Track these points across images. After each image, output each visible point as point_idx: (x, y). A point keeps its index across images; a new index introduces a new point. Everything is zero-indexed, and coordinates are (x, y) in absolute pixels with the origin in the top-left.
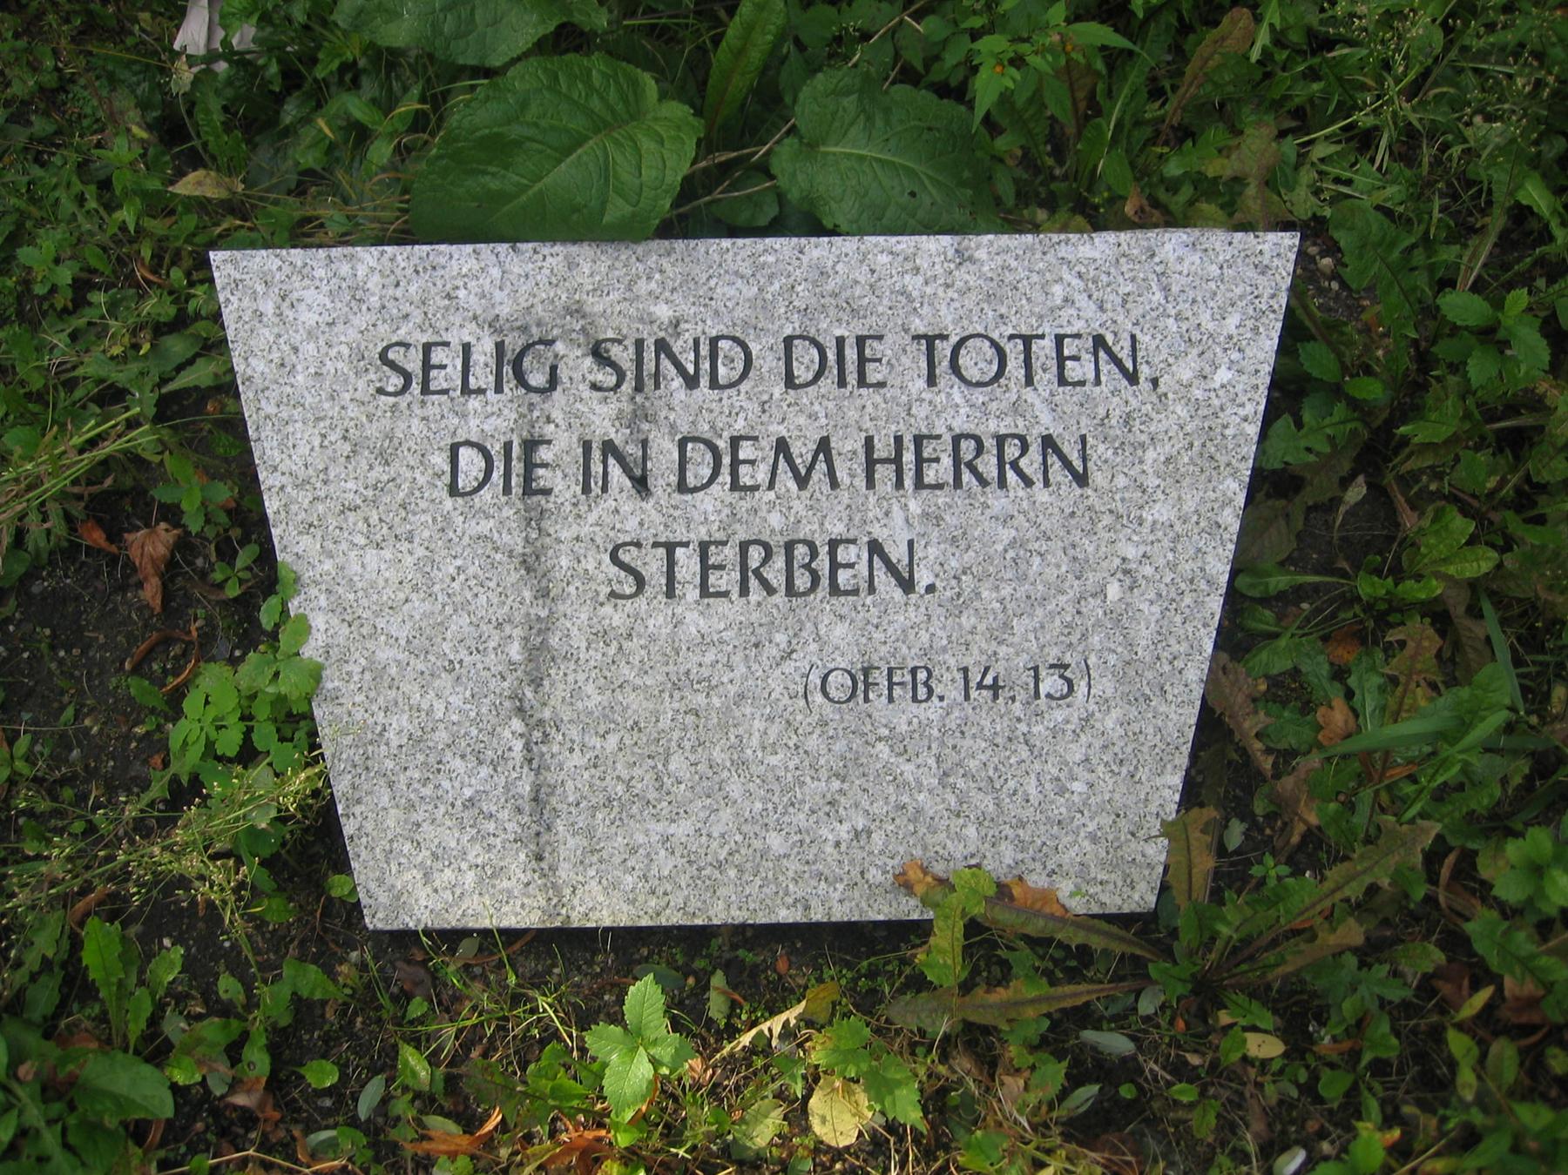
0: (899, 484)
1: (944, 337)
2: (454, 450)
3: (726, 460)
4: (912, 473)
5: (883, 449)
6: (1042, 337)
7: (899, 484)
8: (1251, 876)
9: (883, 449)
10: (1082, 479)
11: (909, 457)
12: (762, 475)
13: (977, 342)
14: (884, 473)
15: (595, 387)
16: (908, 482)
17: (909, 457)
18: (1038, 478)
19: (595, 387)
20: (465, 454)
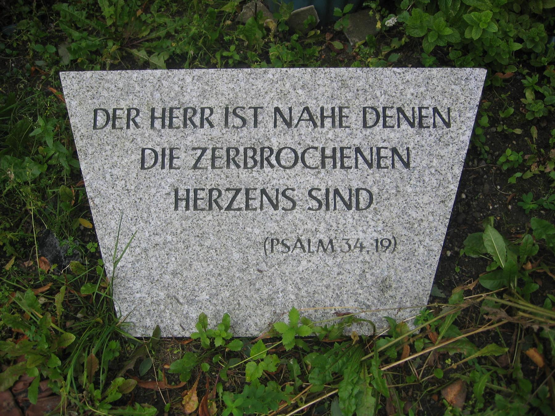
0: (335, 166)
1: (39, 388)
2: (96, 111)
3: (381, 115)
4: (376, 162)
5: (182, 193)
6: (255, 189)
7: (335, 166)
8: (231, 20)
9: (182, 193)
10: (407, 165)
11: (338, 155)
12: (389, 162)
13: (288, 164)
14: (329, 162)
15: (293, 190)
16: (339, 165)
17: (338, 155)
18: (242, 165)
19: (293, 190)
20: (100, 113)
